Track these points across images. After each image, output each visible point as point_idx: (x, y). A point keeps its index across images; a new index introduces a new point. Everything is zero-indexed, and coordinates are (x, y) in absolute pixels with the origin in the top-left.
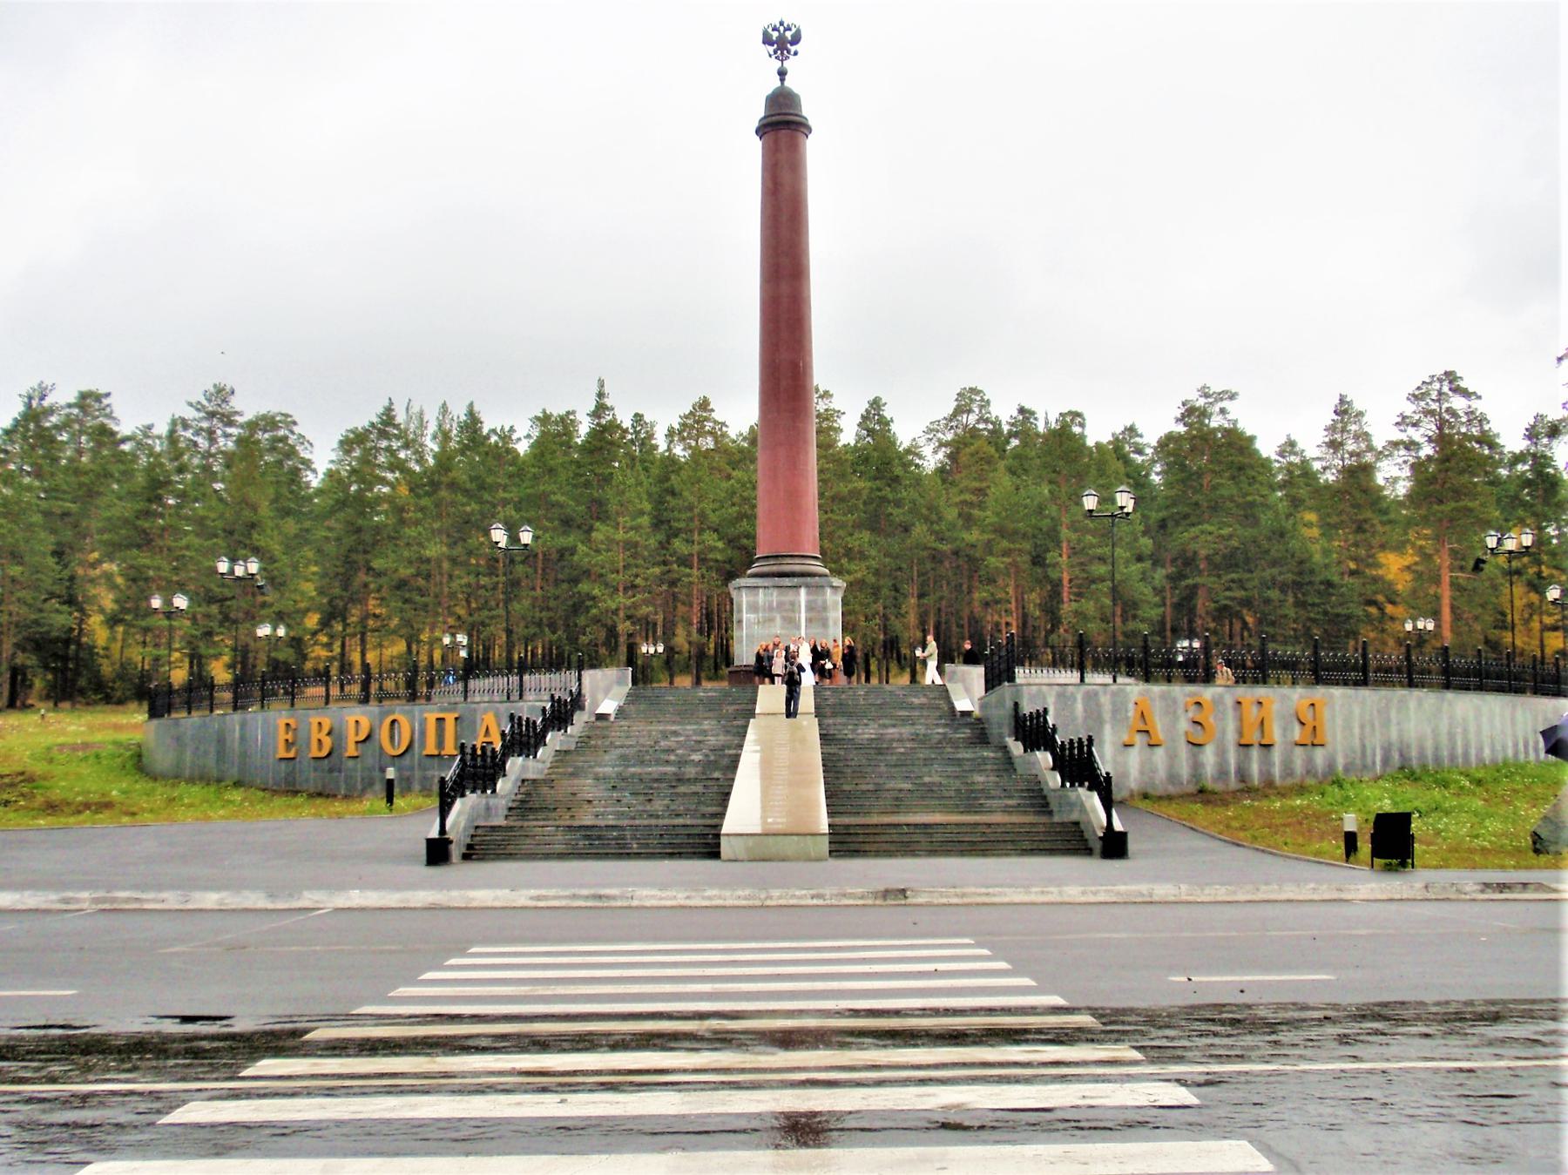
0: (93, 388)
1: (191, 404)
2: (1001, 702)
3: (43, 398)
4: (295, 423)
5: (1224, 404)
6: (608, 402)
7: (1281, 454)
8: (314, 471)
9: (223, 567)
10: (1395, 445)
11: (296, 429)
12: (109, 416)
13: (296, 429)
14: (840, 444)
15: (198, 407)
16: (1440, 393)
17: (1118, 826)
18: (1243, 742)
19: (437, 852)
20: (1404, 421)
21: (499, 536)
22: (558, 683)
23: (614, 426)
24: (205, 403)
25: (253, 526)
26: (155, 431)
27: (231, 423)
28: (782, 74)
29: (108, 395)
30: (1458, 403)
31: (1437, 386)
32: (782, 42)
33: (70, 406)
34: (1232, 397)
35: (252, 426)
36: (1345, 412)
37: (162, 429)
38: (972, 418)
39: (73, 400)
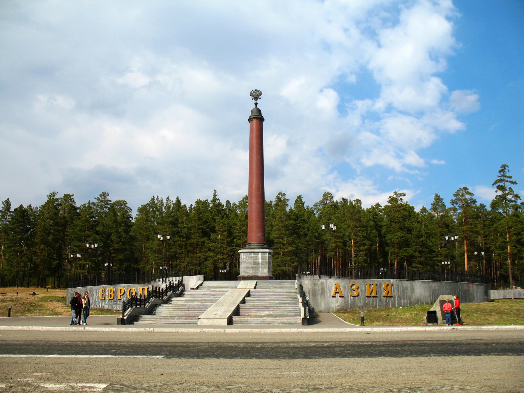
3: (54, 196)
5: (402, 197)
6: (217, 197)
7: (421, 212)
8: (132, 218)
11: (127, 205)
12: (74, 202)
13: (127, 205)
14: (134, 214)
15: (97, 199)
16: (463, 194)
20: (453, 202)
23: (220, 204)
24: (100, 198)
27: (107, 204)
28: (256, 104)
30: (468, 197)
31: (461, 192)
32: (256, 95)
33: (61, 199)
34: (404, 195)
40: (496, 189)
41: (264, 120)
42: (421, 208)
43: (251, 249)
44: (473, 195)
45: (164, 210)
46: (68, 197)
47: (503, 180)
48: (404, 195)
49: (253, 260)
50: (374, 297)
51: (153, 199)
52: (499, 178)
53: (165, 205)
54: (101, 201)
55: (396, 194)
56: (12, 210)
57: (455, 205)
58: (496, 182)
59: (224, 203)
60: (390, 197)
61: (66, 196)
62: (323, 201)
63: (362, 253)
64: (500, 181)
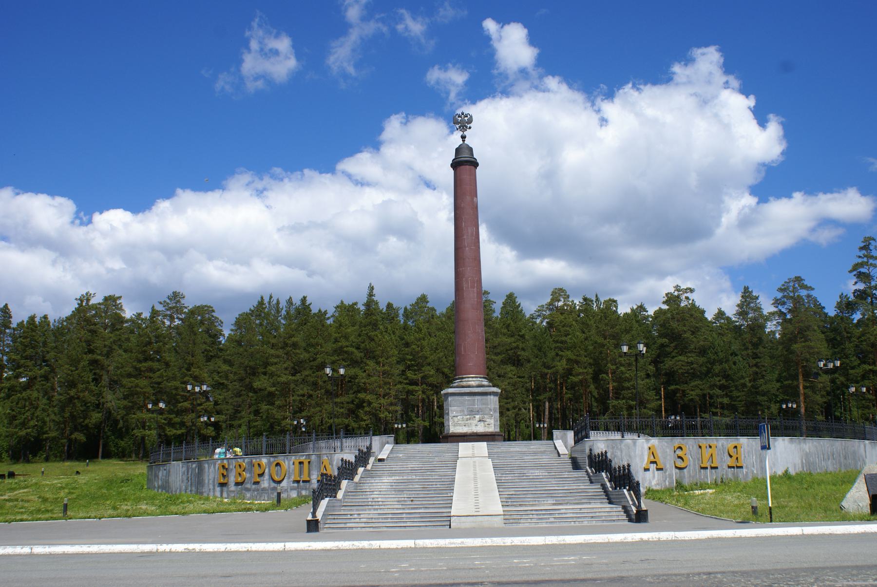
0: (112, 294)
1: (161, 303)
2: (583, 451)
3: (88, 300)
4: (213, 311)
5: (688, 295)
6: (375, 298)
8: (224, 335)
9: (189, 387)
10: (773, 314)
17: (644, 507)
18: (703, 466)
19: (313, 526)
21: (328, 371)
22: (363, 443)
25: (191, 364)
26: (143, 316)
29: (120, 298)
31: (791, 284)
34: (692, 291)
35: (192, 312)
36: (749, 297)
37: (146, 315)
38: (560, 304)
39: (101, 301)
40: (855, 280)
41: (452, 165)
42: (716, 311)
43: (463, 387)
44: (813, 289)
45: (283, 321)
46: (111, 301)
47: (866, 263)
48: (692, 291)
49: (472, 410)
50: (304, 481)
51: (261, 303)
52: (860, 260)
53: (283, 312)
54: (171, 308)
55: (677, 288)
56: (14, 325)
57: (780, 307)
58: (856, 267)
59: (383, 306)
60: (667, 295)
61: (106, 299)
62: (550, 304)
63: (698, 391)
64: (862, 265)
